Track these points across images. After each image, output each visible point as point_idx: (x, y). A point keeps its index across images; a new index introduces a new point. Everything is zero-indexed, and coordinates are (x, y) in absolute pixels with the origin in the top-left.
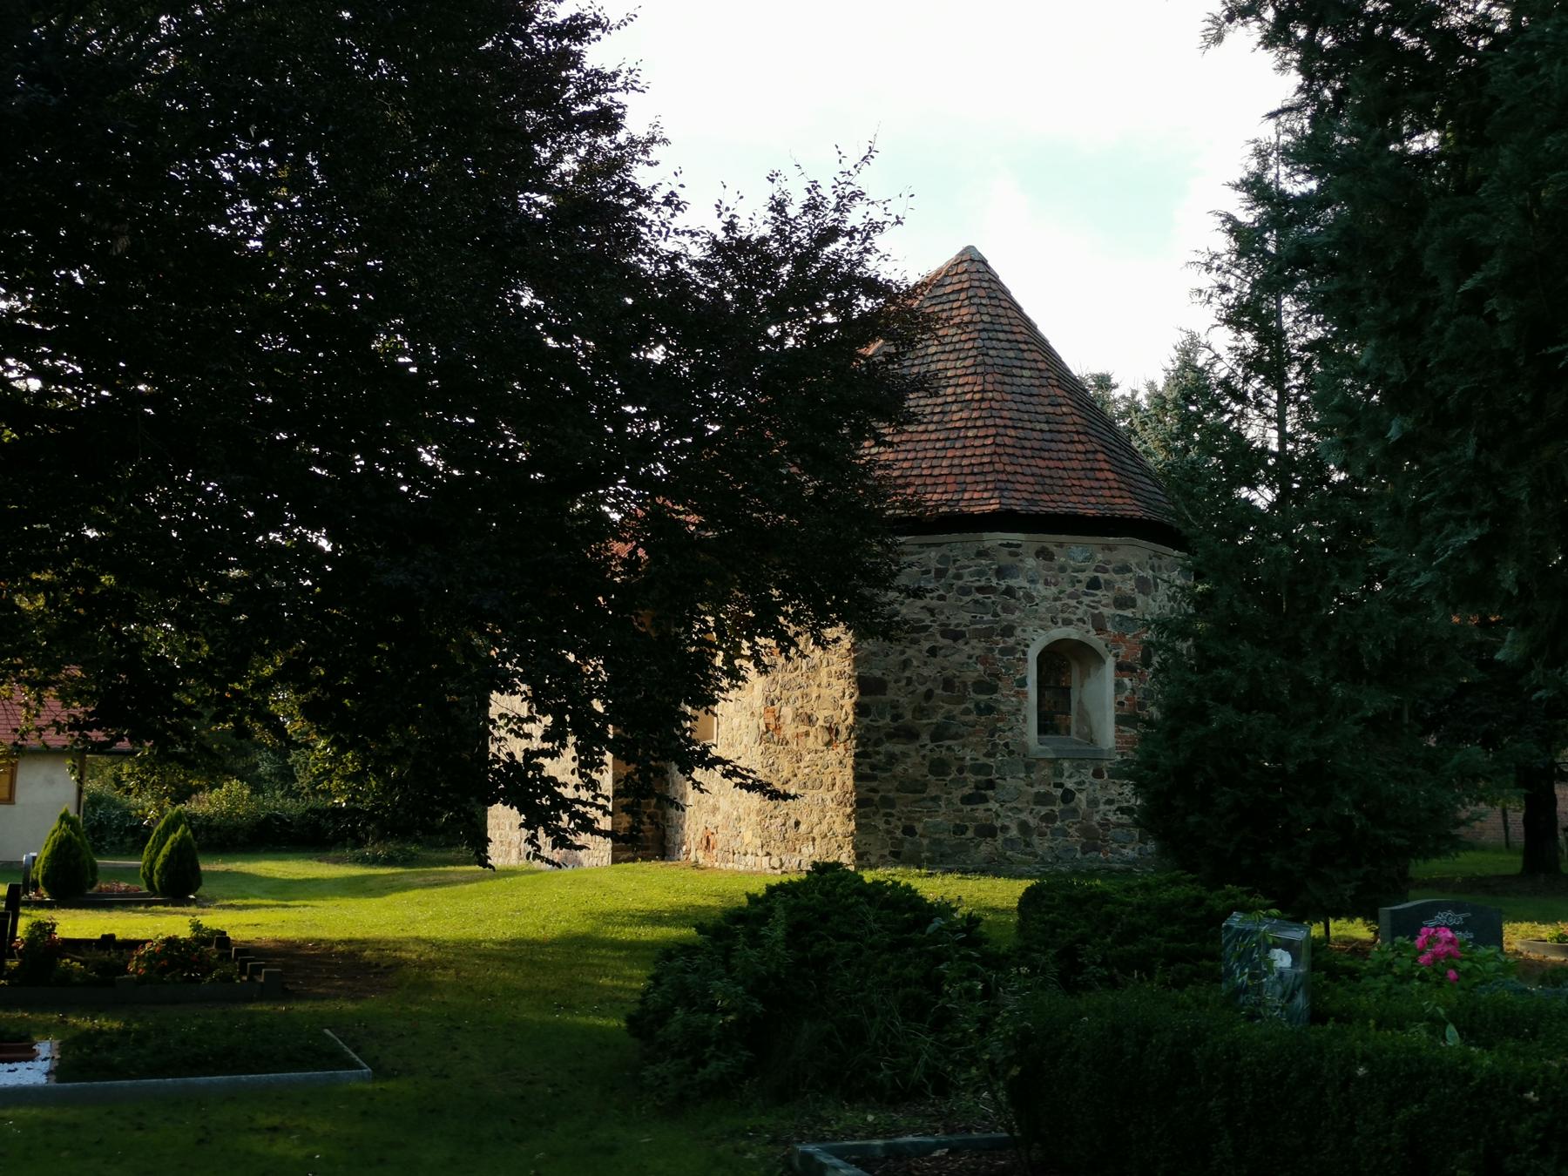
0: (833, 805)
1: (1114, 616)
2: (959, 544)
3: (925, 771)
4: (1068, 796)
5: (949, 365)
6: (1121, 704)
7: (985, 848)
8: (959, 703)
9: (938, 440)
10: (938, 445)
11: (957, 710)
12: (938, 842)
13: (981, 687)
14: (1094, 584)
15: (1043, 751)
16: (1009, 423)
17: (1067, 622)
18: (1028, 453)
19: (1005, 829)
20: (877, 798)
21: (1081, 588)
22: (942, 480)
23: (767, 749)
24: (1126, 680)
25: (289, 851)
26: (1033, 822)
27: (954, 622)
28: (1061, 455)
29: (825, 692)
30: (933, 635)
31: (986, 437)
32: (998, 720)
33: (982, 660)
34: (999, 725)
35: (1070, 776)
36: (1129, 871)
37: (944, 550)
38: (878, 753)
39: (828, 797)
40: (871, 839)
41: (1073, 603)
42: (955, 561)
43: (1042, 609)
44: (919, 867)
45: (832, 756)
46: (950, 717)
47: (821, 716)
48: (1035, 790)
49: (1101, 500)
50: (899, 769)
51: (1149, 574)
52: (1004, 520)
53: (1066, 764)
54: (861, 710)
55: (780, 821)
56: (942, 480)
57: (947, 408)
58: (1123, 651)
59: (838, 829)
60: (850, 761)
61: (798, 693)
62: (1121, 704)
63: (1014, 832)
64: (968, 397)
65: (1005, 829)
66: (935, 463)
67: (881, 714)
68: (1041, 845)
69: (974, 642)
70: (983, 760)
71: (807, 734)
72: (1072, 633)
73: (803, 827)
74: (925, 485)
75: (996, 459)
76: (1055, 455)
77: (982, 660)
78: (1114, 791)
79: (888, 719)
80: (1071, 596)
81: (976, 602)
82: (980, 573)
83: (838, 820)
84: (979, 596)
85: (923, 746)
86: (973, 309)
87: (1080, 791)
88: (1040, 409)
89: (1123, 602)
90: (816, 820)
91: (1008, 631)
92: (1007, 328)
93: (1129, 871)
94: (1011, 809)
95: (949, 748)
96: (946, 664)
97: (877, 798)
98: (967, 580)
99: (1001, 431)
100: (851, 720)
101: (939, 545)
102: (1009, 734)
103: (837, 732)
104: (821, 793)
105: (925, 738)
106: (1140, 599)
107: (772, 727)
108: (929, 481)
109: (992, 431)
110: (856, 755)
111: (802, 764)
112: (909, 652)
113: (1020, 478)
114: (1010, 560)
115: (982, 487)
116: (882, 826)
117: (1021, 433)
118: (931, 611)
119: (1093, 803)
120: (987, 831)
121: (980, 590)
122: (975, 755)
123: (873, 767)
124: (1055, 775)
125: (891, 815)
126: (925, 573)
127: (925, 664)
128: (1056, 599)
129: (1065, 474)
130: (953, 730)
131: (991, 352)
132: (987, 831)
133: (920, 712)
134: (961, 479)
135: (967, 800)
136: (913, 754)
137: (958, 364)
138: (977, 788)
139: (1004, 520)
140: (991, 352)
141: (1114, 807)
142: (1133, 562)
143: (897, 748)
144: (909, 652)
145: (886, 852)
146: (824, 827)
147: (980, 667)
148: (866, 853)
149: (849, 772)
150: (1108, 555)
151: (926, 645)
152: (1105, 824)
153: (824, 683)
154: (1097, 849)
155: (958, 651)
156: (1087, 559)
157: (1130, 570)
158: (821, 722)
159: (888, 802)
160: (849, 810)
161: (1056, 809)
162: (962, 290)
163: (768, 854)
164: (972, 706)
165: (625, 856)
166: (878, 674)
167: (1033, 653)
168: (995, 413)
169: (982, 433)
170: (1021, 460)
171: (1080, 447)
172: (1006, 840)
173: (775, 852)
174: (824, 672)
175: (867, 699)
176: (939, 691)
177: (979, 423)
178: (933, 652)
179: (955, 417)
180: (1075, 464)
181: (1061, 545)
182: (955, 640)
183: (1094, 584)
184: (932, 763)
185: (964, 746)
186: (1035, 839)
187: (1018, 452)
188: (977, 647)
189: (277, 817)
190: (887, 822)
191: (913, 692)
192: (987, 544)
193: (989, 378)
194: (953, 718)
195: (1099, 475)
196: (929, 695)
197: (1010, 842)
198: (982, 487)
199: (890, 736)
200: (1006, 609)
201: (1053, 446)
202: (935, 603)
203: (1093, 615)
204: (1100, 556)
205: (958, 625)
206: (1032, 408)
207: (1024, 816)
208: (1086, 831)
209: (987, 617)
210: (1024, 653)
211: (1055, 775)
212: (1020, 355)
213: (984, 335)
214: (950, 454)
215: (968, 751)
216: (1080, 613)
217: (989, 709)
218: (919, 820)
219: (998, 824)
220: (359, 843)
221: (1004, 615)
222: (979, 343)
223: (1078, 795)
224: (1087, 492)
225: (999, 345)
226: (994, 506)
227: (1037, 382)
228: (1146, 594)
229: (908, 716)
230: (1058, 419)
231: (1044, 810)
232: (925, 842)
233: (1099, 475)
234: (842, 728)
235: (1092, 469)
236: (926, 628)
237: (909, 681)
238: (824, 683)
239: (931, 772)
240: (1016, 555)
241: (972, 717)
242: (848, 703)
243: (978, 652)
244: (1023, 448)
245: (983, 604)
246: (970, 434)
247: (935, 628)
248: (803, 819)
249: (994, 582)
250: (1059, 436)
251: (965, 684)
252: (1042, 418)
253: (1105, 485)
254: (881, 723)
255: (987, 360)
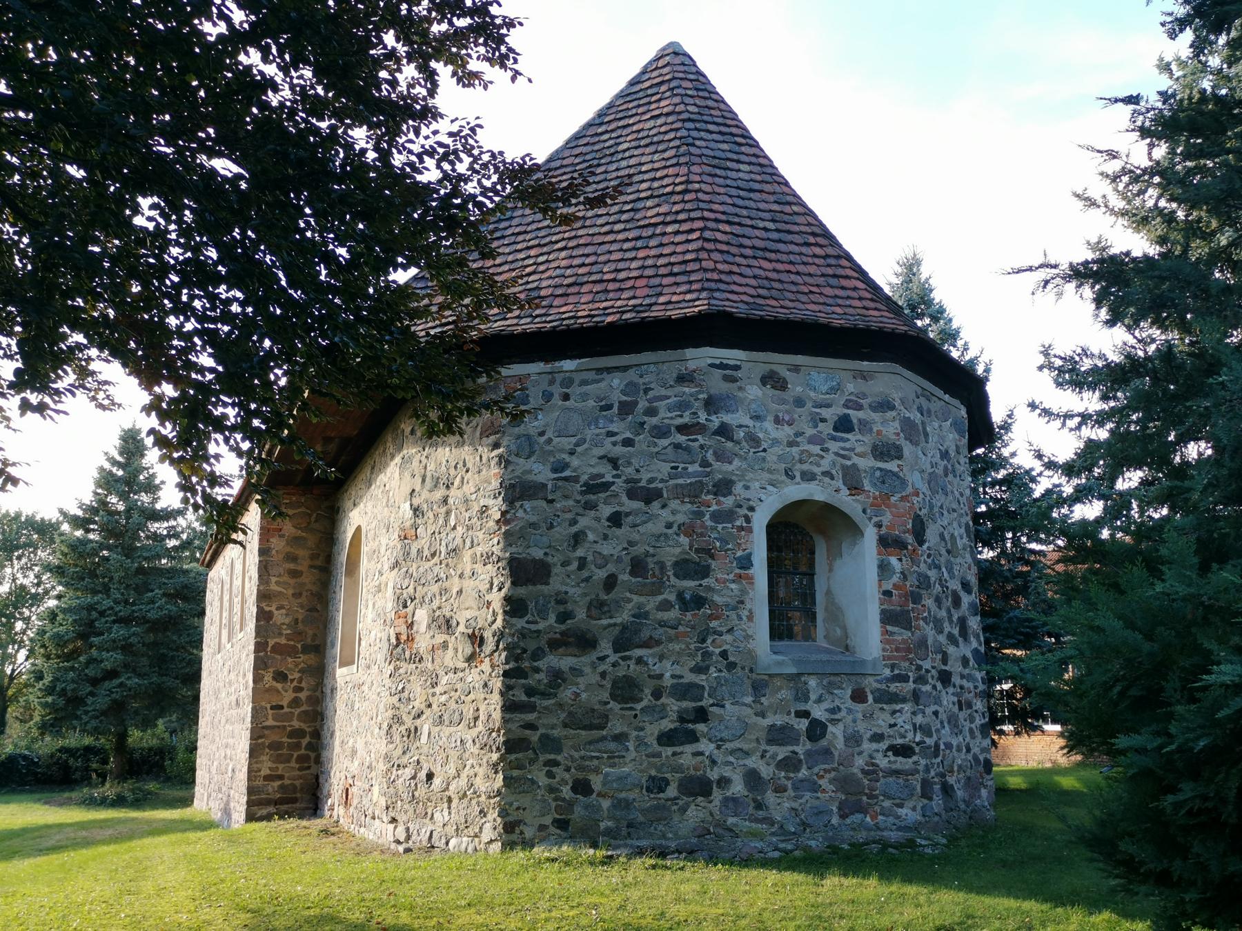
0: (475, 750)
1: (874, 469)
2: (654, 367)
3: (605, 695)
4: (817, 730)
5: (644, 159)
6: (887, 593)
7: (695, 813)
8: (653, 593)
9: (627, 240)
10: (626, 246)
11: (651, 603)
12: (626, 805)
13: (686, 568)
14: (844, 425)
15: (779, 664)
16: (723, 217)
17: (808, 477)
18: (748, 252)
19: (724, 782)
20: (534, 737)
21: (826, 429)
22: (629, 284)
23: (397, 669)
24: (894, 560)
25: (14, 791)
26: (766, 771)
27: (645, 476)
28: (792, 257)
29: (468, 584)
30: (616, 495)
31: (692, 231)
32: (711, 617)
33: (687, 529)
34: (714, 624)
35: (820, 700)
36: (911, 843)
37: (632, 375)
38: (537, 670)
39: (469, 736)
40: (525, 801)
41: (816, 449)
42: (646, 391)
43: (771, 456)
44: (595, 846)
45: (473, 677)
46: (640, 615)
47: (462, 617)
48: (767, 722)
49: (851, 311)
50: (566, 694)
51: (916, 417)
52: (712, 328)
53: (812, 682)
54: (514, 607)
55: (408, 772)
56: (629, 284)
57: (640, 205)
58: (887, 519)
59: (482, 785)
60: (497, 684)
61: (435, 588)
62: (887, 593)
63: (738, 788)
64: (669, 189)
65: (724, 782)
66: (621, 265)
67: (543, 614)
68: (779, 806)
69: (674, 504)
70: (690, 678)
71: (445, 645)
72: (816, 492)
73: (437, 781)
74: (606, 291)
75: (704, 255)
76: (784, 257)
77: (687, 529)
78: (882, 721)
79: (552, 619)
80: (811, 441)
81: (677, 446)
82: (682, 406)
83: (481, 771)
84: (681, 439)
85: (602, 659)
86: (677, 100)
87: (835, 722)
88: (762, 206)
89: (885, 451)
90: (453, 771)
91: (724, 487)
92: (720, 120)
93: (911, 843)
94: (732, 752)
95: (640, 661)
96: (636, 537)
97: (534, 737)
98: (665, 416)
99: (711, 224)
100: (499, 623)
101: (625, 369)
102: (728, 638)
103: (482, 638)
104: (461, 732)
105: (605, 647)
106: (907, 449)
107: (404, 637)
108: (611, 286)
109: (700, 224)
110: (506, 674)
111: (438, 690)
112: (583, 522)
113: (736, 278)
114: (725, 387)
115: (684, 288)
116: (543, 780)
117: (737, 230)
118: (614, 462)
119: (853, 739)
120: (698, 787)
121: (682, 429)
122: (678, 670)
123: (530, 692)
124: (797, 699)
125: (557, 764)
126: (603, 408)
127: (605, 537)
128: (791, 444)
129: (798, 279)
130: (645, 634)
131: (698, 143)
132: (698, 787)
133: (598, 607)
134: (656, 281)
135: (667, 738)
136: (587, 670)
137: (656, 157)
138: (682, 720)
139: (712, 328)
140: (698, 143)
141: (883, 745)
142: (896, 397)
143: (565, 662)
144: (583, 522)
145: (547, 821)
146: (463, 782)
147: (684, 540)
148: (518, 823)
149: (496, 699)
150: (861, 386)
151: (606, 511)
152: (871, 771)
153: (468, 572)
154: (863, 810)
155: (651, 518)
156: (833, 390)
157: (893, 408)
158: (461, 628)
159: (552, 745)
160: (495, 757)
161: (799, 749)
162: (662, 83)
163: (394, 820)
164: (672, 598)
165: (264, 812)
166: (538, 554)
167: (760, 521)
168: (702, 205)
169: (685, 227)
170: (739, 260)
171: (818, 251)
172: (726, 800)
173: (402, 818)
174: (467, 556)
175: (522, 591)
176: (624, 577)
177: (681, 217)
178: (616, 520)
179: (650, 213)
180: (812, 269)
181: (796, 369)
182: (648, 502)
183: (844, 425)
184: (615, 683)
185: (662, 657)
186: (770, 797)
187: (734, 250)
188: (680, 511)
189: (25, 757)
190: (550, 775)
191: (587, 580)
192: (692, 365)
193: (695, 169)
194: (646, 615)
195: (844, 283)
196: (610, 583)
197: (732, 803)
198: (684, 288)
199: (554, 645)
200: (719, 456)
201: (781, 247)
202: (619, 450)
203: (844, 467)
204: (850, 387)
205: (651, 481)
206: (752, 204)
207: (753, 762)
208: (845, 783)
209: (692, 468)
210: (748, 520)
211: (797, 699)
212: (737, 148)
213: (690, 125)
214: (641, 254)
215: (667, 664)
216: (826, 464)
217: (699, 602)
218: (597, 771)
219: (714, 775)
220: (85, 780)
221: (717, 465)
222: (683, 133)
223: (831, 728)
224: (830, 301)
225: (710, 137)
226: (701, 306)
227: (758, 178)
228: (915, 443)
229: (581, 614)
230: (786, 218)
231: (782, 752)
232: (606, 804)
233: (844, 283)
234: (488, 635)
235: (835, 276)
236: (606, 486)
237: (583, 563)
238: (468, 572)
239: (613, 696)
240: (733, 380)
241: (673, 614)
242: (496, 598)
243: (680, 518)
244: (741, 246)
245: (687, 449)
246: (669, 229)
247: (619, 486)
248: (437, 770)
249: (702, 417)
250: (789, 237)
251: (662, 566)
252: (767, 216)
253: (854, 294)
254: (541, 626)
255: (693, 150)
